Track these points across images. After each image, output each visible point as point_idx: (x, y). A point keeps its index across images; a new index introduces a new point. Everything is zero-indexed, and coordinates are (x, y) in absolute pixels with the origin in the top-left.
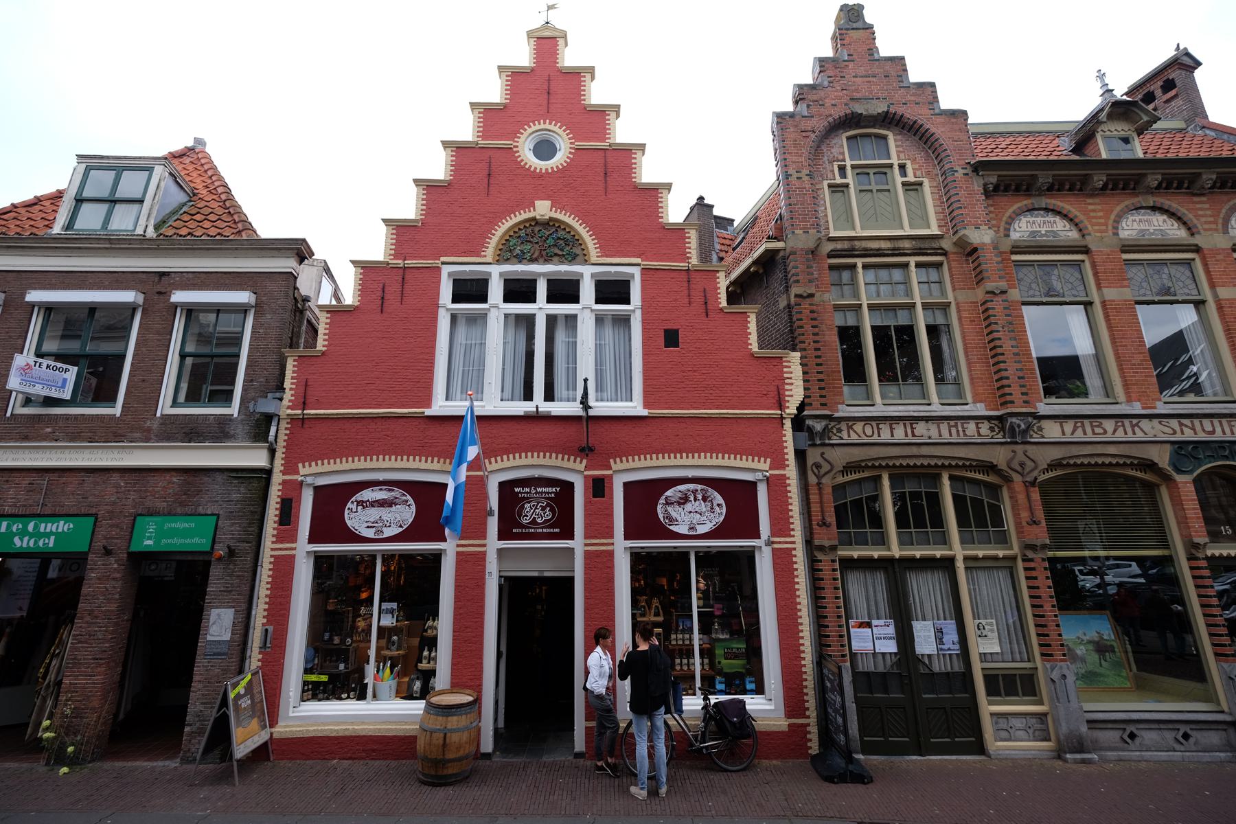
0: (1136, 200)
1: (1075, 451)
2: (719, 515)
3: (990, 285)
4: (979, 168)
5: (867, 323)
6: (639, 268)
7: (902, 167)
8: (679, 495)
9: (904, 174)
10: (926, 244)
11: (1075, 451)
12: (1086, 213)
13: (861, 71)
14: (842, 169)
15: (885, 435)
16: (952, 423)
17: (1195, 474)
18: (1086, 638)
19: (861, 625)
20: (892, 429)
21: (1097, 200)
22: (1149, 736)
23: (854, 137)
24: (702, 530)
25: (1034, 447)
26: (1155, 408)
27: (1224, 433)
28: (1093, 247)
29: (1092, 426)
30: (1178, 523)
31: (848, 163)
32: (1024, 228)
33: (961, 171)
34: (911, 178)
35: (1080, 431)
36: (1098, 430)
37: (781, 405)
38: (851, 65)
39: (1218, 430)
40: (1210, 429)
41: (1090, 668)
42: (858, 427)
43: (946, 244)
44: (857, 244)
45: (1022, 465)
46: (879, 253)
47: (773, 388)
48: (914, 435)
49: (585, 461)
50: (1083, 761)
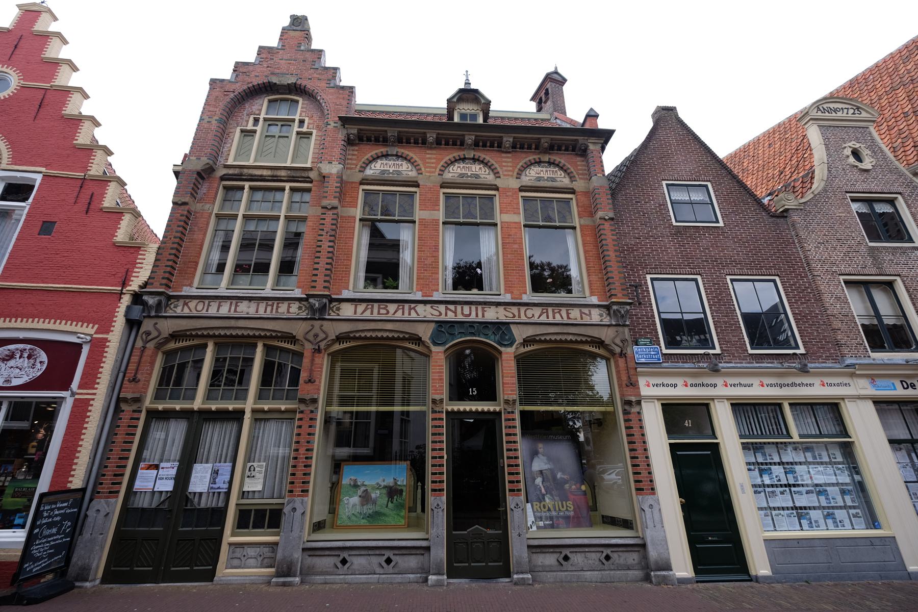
0: (463, 153)
1: (361, 326)
2: (39, 370)
4: (345, 121)
6: (41, 175)
7: (302, 122)
8: (7, 353)
10: (298, 174)
11: (361, 326)
13: (285, 57)
14: (256, 121)
15: (213, 311)
17: (447, 346)
18: (383, 484)
19: (149, 467)
20: (289, 307)
21: (434, 152)
22: (358, 562)
23: (275, 100)
24: (16, 382)
25: (330, 323)
27: (477, 316)
28: (421, 183)
29: (379, 308)
31: (263, 116)
33: (333, 124)
34: (305, 129)
35: (369, 311)
36: (383, 311)
37: (124, 284)
38: (281, 52)
39: (474, 314)
41: (378, 508)
42: (192, 304)
43: (312, 175)
44: (245, 171)
45: (316, 336)
47: (123, 271)
49: (96, 326)
50: (284, 584)
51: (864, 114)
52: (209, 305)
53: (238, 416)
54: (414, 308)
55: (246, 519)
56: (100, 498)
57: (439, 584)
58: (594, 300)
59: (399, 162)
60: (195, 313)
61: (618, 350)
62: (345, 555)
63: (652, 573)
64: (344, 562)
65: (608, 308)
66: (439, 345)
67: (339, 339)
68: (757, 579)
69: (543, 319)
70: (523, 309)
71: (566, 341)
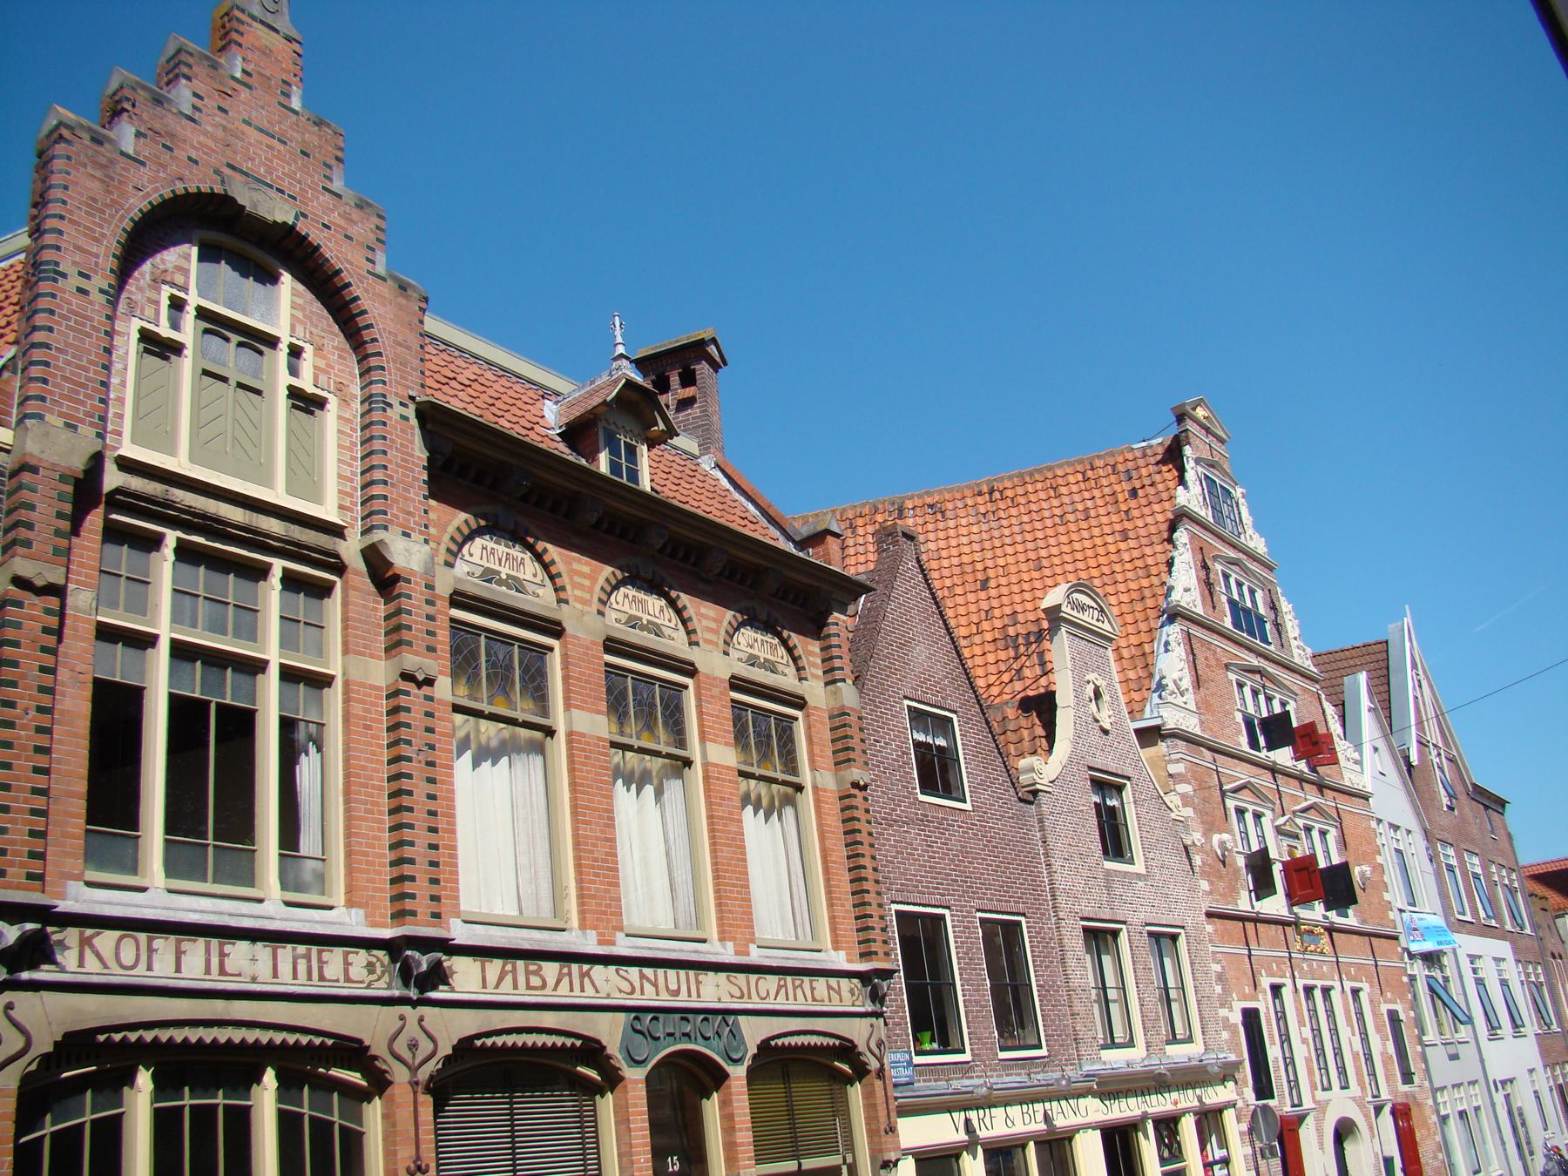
3: (412, 660)
5: (159, 683)
7: (295, 352)
9: (294, 371)
12: (568, 563)
14: (177, 305)
15: (162, 971)
16: (302, 949)
17: (649, 1067)
20: (179, 954)
26: (613, 943)
28: (570, 628)
29: (528, 973)
30: (869, 1131)
31: (193, 300)
32: (475, 559)
34: (306, 384)
36: (535, 981)
38: (244, 94)
40: (673, 987)
45: (413, 1046)
48: (222, 972)
51: (1106, 626)
52: (698, 983)
54: (587, 974)
58: (840, 960)
61: (874, 1064)
65: (393, 947)
66: (639, 1063)
70: (753, 977)
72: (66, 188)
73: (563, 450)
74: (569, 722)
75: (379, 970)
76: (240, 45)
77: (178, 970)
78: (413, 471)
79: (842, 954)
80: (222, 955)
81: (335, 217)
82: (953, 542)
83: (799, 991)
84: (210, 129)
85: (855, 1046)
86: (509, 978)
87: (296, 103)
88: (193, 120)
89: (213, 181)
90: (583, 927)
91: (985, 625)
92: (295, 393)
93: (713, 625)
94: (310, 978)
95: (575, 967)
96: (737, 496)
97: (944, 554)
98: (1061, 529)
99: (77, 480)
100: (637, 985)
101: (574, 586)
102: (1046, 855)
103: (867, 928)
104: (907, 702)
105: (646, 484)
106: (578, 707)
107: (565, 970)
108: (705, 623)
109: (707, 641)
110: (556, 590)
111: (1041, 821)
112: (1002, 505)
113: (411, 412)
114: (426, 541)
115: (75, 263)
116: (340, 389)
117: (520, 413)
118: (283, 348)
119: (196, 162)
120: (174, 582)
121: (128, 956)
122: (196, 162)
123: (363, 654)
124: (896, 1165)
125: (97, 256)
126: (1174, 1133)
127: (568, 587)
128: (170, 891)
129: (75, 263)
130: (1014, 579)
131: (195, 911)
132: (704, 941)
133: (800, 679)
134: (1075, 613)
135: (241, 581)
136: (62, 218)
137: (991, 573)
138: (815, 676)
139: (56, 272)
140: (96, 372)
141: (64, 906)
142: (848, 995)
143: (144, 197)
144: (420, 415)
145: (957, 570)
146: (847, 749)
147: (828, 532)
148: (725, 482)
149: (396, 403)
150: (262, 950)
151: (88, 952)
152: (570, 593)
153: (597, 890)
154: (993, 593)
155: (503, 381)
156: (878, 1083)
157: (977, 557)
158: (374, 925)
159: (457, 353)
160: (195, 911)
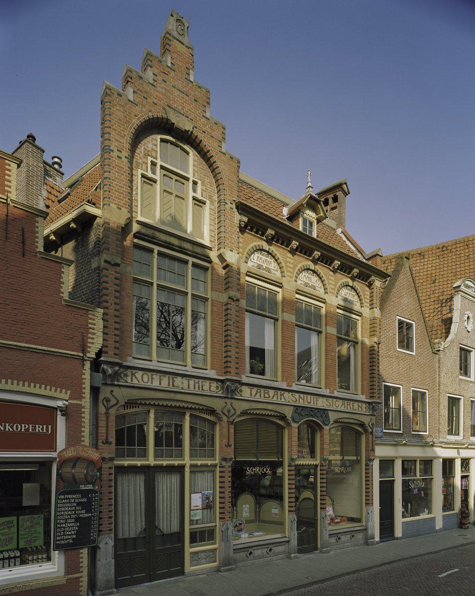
1: (255, 405)
3: (232, 293)
7: (195, 183)
9: (195, 191)
11: (255, 405)
14: (154, 164)
15: (156, 384)
16: (197, 380)
22: (258, 552)
26: (291, 386)
28: (285, 285)
29: (264, 393)
31: (159, 162)
32: (255, 261)
36: (267, 395)
37: (84, 351)
38: (172, 73)
40: (309, 401)
42: (139, 374)
45: (229, 411)
46: (169, 246)
49: (69, 392)
52: (317, 400)
53: (180, 469)
54: (283, 395)
55: (196, 537)
56: (105, 534)
57: (296, 558)
59: (268, 259)
60: (142, 384)
61: (370, 430)
62: (251, 550)
63: (369, 541)
64: (251, 553)
67: (244, 413)
68: (398, 539)
69: (342, 409)
70: (335, 400)
71: (350, 423)
72: (110, 115)
73: (287, 223)
74: (283, 317)
75: (220, 388)
76: (170, 51)
77: (160, 384)
78: (234, 228)
79: (364, 396)
80: (173, 381)
81: (207, 128)
82: (426, 267)
83: (349, 406)
84: (160, 89)
85: (365, 424)
86: (259, 394)
87: (192, 79)
88: (154, 86)
89: (163, 113)
90: (282, 381)
91: (432, 296)
92: (194, 199)
93: (333, 287)
94: (199, 389)
95: (279, 392)
96: (348, 243)
97: (422, 271)
98: (467, 261)
99: (122, 228)
100: (298, 399)
101: (287, 271)
102: (439, 372)
103: (373, 389)
104: (398, 317)
105: (315, 235)
106: (286, 312)
107: (276, 393)
108: (331, 286)
109: (330, 292)
110: (324, 289)
111: (439, 360)
112: (446, 252)
113: (234, 206)
114: (238, 253)
115: (116, 146)
116: (210, 198)
117: (274, 210)
118: (191, 181)
119: (156, 104)
120: (157, 266)
121: (145, 379)
122: (156, 104)
123: (217, 291)
124: (373, 460)
125: (123, 143)
126: (468, 464)
127: (285, 271)
128: (158, 362)
129: (116, 146)
130: (445, 279)
131: (165, 368)
132: (321, 388)
133: (361, 307)
134: (466, 289)
135: (179, 263)
136: (110, 127)
137: (437, 277)
138: (366, 306)
139: (109, 149)
140: (126, 189)
141: (125, 364)
142: (364, 409)
143: (138, 119)
144: (237, 208)
145: (425, 277)
146: (374, 331)
147: (377, 255)
148: (344, 238)
149: (229, 203)
150: (185, 381)
151: (134, 378)
152: (286, 274)
153: (288, 370)
154: (437, 284)
155: (270, 200)
156: (371, 436)
157: (434, 272)
158: (218, 375)
159: (254, 189)
160: (165, 368)
